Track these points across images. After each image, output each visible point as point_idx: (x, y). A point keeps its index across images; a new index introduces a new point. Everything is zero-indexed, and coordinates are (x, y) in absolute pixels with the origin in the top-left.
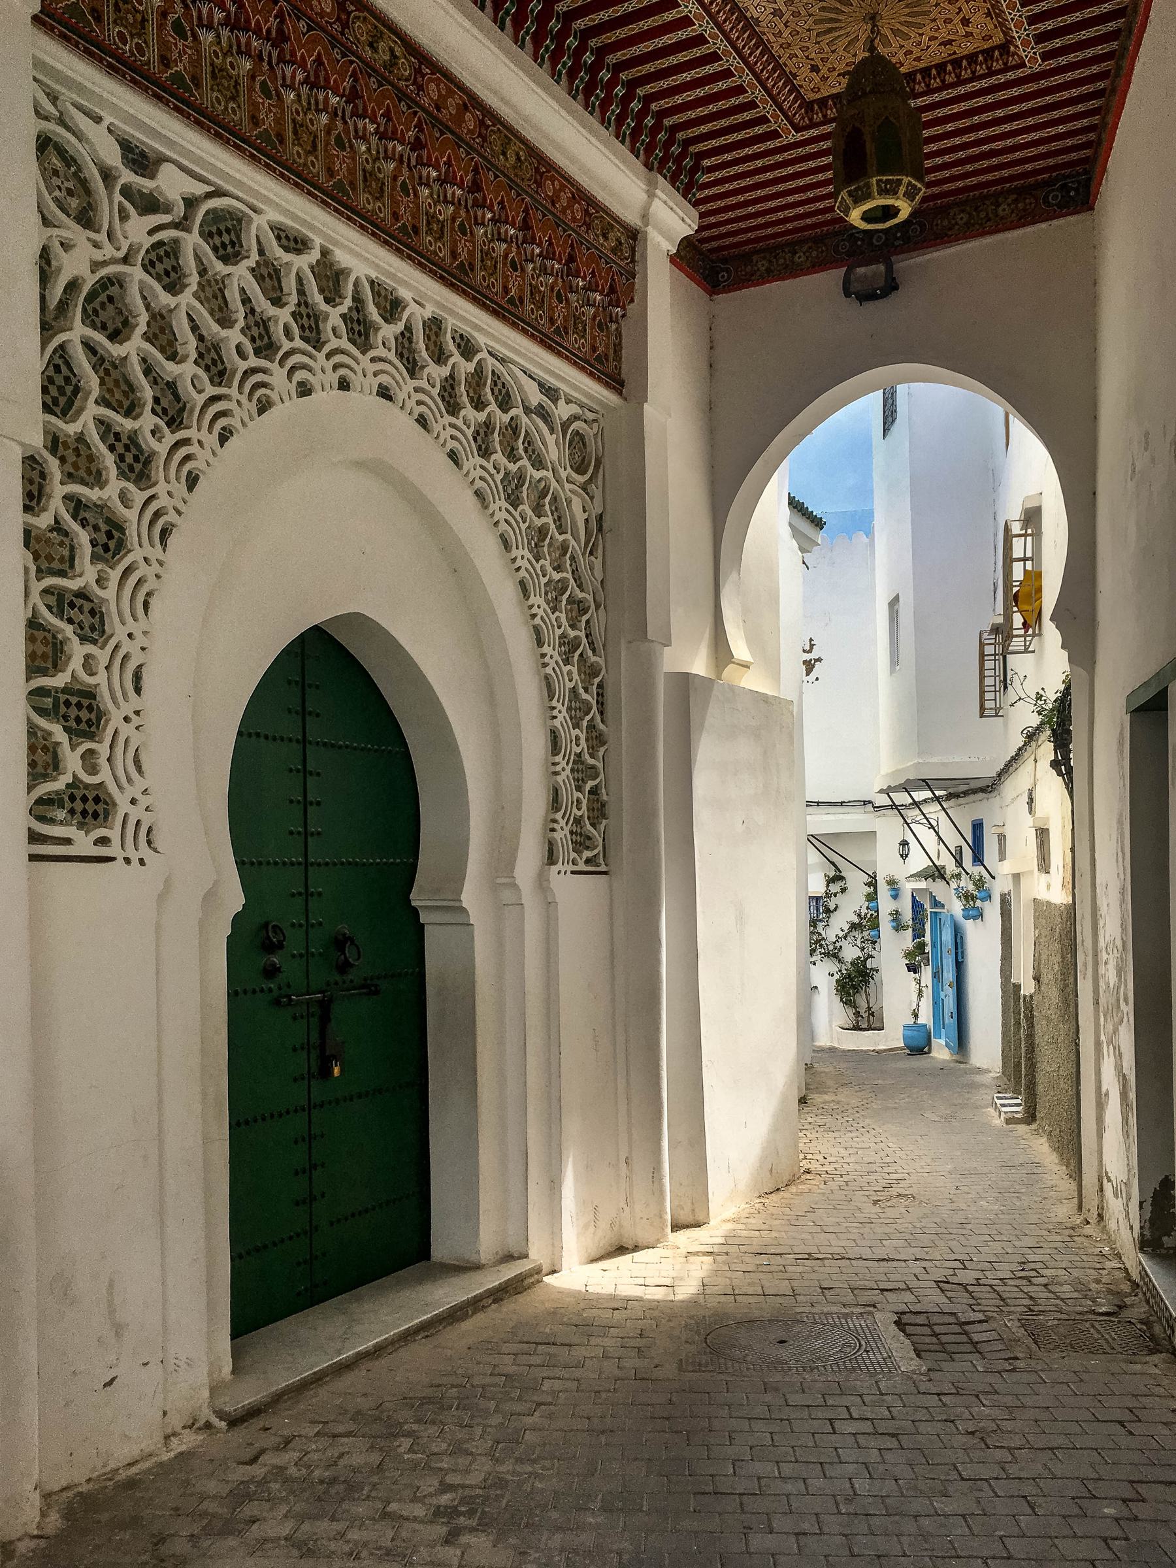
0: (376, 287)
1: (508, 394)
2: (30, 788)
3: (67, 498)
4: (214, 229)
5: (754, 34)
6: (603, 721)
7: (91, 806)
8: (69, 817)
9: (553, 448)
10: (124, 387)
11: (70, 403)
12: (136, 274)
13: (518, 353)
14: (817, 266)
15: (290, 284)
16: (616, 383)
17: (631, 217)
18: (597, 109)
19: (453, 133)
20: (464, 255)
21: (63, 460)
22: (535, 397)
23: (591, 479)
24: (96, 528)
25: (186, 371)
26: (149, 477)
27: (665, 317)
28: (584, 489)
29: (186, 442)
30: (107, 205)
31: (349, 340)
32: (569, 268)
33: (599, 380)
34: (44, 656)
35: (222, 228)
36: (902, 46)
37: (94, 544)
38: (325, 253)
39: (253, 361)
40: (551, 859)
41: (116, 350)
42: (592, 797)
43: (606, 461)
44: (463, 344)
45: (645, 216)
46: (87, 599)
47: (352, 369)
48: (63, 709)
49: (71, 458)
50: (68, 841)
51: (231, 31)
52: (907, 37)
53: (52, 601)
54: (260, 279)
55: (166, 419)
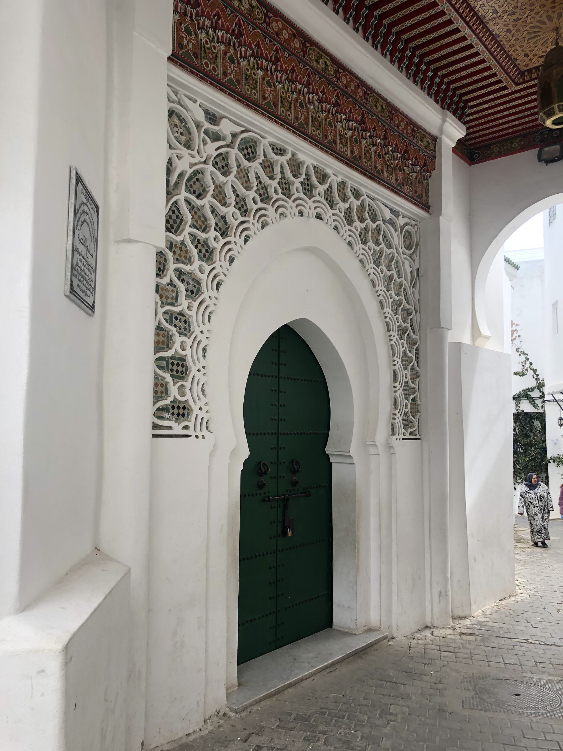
0: (316, 169)
2: (154, 404)
5: (496, 42)
6: (418, 366)
7: (181, 411)
9: (396, 239)
10: (203, 219)
11: (179, 227)
12: (210, 168)
14: (523, 149)
15: (277, 170)
16: (426, 207)
17: (434, 131)
21: (174, 253)
24: (188, 283)
25: (230, 211)
26: (212, 259)
28: (411, 257)
30: (197, 137)
34: (163, 342)
37: (187, 290)
39: (260, 205)
41: (199, 202)
42: (413, 402)
43: (421, 244)
44: (355, 193)
45: (441, 131)
46: (183, 316)
48: (170, 366)
49: (178, 251)
50: (170, 428)
53: (168, 317)
54: (264, 168)
55: (221, 232)
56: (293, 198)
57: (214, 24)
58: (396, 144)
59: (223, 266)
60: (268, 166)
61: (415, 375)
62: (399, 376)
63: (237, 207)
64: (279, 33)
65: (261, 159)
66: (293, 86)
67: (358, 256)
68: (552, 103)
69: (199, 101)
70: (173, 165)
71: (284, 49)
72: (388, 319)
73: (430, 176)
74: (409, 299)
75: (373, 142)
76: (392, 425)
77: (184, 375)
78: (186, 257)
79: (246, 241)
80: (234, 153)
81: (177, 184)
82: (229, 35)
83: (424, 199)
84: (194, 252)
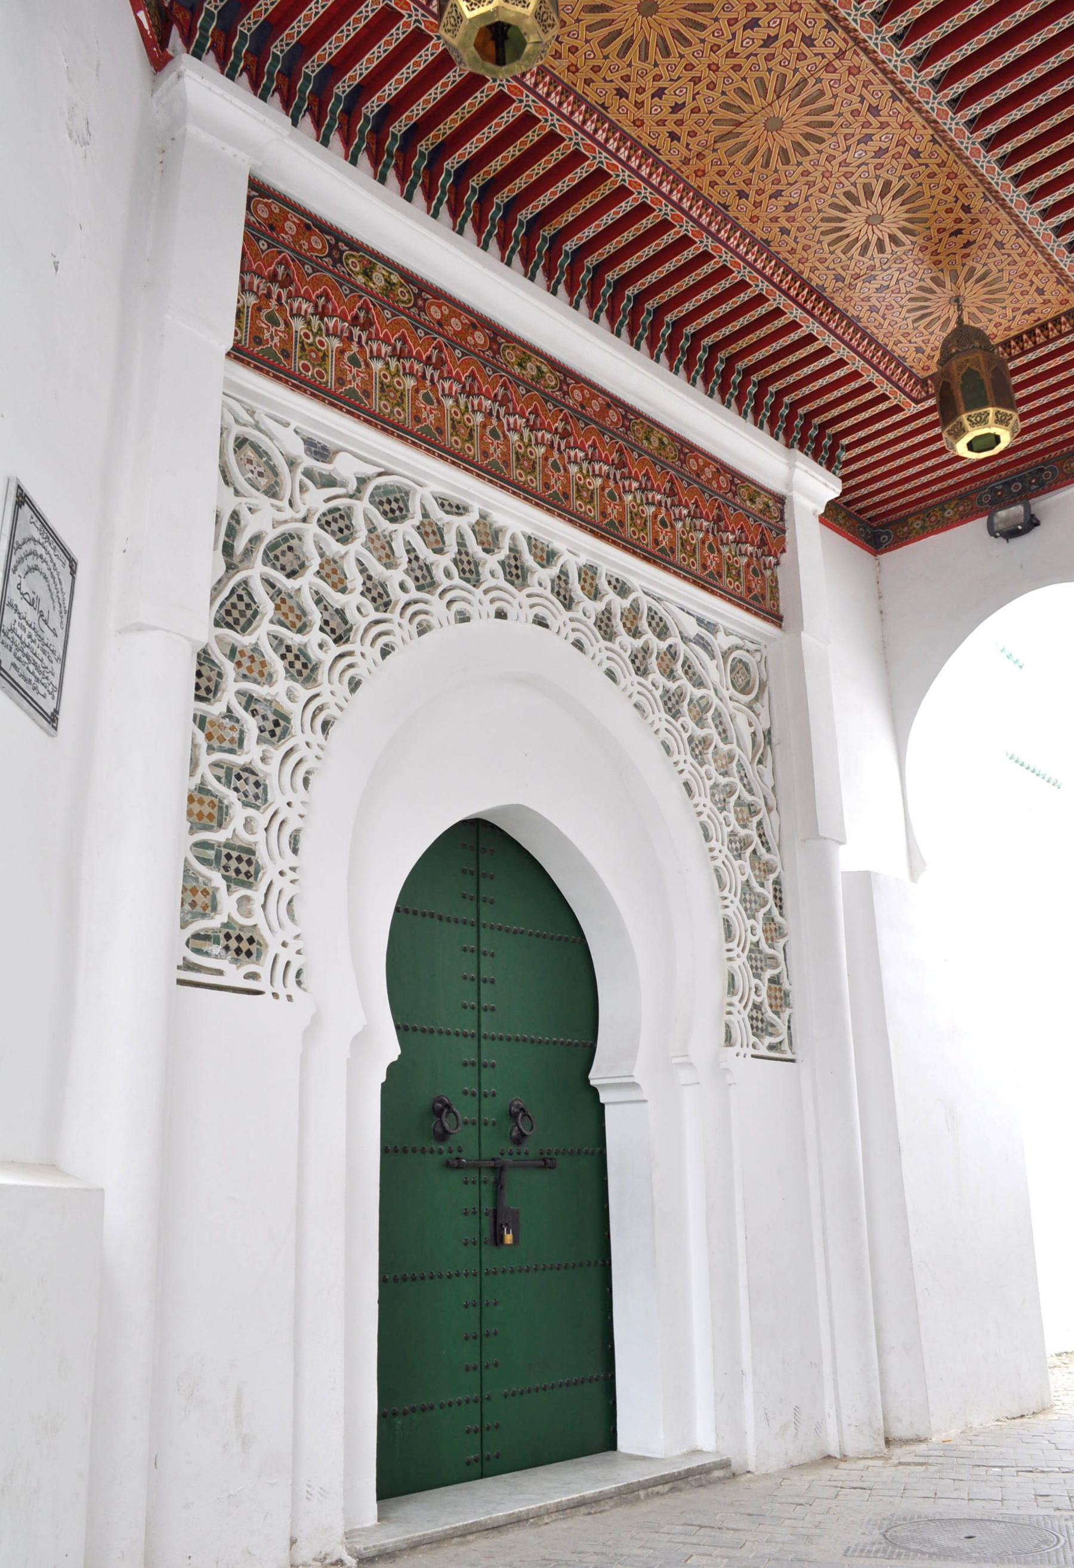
0: (533, 542)
1: (666, 627)
2: (184, 925)
3: (239, 693)
4: (384, 499)
5: (857, 329)
6: (781, 915)
7: (243, 945)
8: (224, 951)
9: (714, 672)
10: (299, 612)
11: (249, 623)
12: (312, 529)
13: (671, 591)
14: (964, 518)
15: (451, 539)
16: (775, 618)
17: (776, 485)
18: (716, 392)
19: (596, 423)
20: (713, 567)
21: (239, 664)
22: (693, 629)
23: (757, 699)
24: (264, 718)
25: (352, 601)
26: (315, 680)
27: (817, 562)
28: (751, 708)
29: (350, 653)
30: (289, 481)
31: (506, 580)
32: (719, 526)
33: (756, 614)
34: (210, 816)
35: (392, 498)
36: (990, 320)
37: (262, 730)
38: (483, 516)
39: (414, 594)
40: (729, 1040)
41: (290, 584)
42: (773, 986)
43: (772, 684)
44: (618, 586)
45: (789, 484)
46: (253, 773)
47: (508, 602)
49: (246, 662)
50: (220, 972)
51: (398, 360)
52: (993, 312)
53: (222, 773)
54: (424, 535)
55: (334, 637)
56: (484, 587)
57: (320, 309)
58: (696, 502)
59: (337, 692)
60: (432, 534)
61: (774, 931)
62: (737, 930)
63: (369, 596)
64: (443, 322)
65: (417, 519)
66: (476, 402)
67: (630, 696)
68: (957, 414)
69: (294, 424)
70: (243, 523)
71: (453, 344)
72: (704, 818)
73: (778, 564)
74: (753, 785)
75: (647, 499)
76: (727, 1026)
77: (252, 880)
78: (261, 674)
79: (385, 653)
80: (362, 509)
81: (248, 552)
82: (347, 324)
83: (765, 602)
84: (279, 666)
